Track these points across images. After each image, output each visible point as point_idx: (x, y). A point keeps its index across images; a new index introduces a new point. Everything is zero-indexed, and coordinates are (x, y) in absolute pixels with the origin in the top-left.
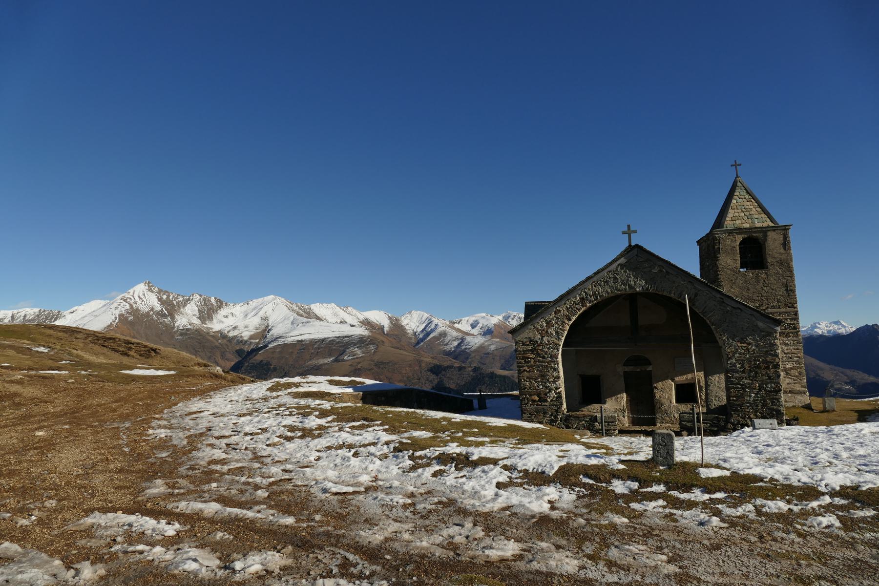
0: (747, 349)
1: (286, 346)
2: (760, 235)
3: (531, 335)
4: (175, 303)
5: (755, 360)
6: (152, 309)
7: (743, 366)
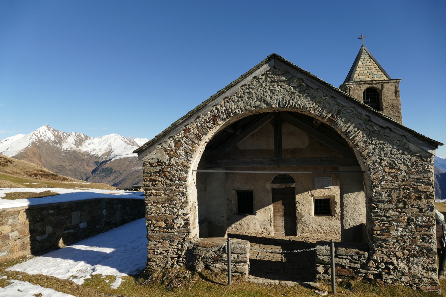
0: (396, 176)
1: (121, 159)
2: (380, 87)
3: (158, 155)
4: (62, 136)
5: (404, 189)
6: (50, 140)
7: (389, 195)
